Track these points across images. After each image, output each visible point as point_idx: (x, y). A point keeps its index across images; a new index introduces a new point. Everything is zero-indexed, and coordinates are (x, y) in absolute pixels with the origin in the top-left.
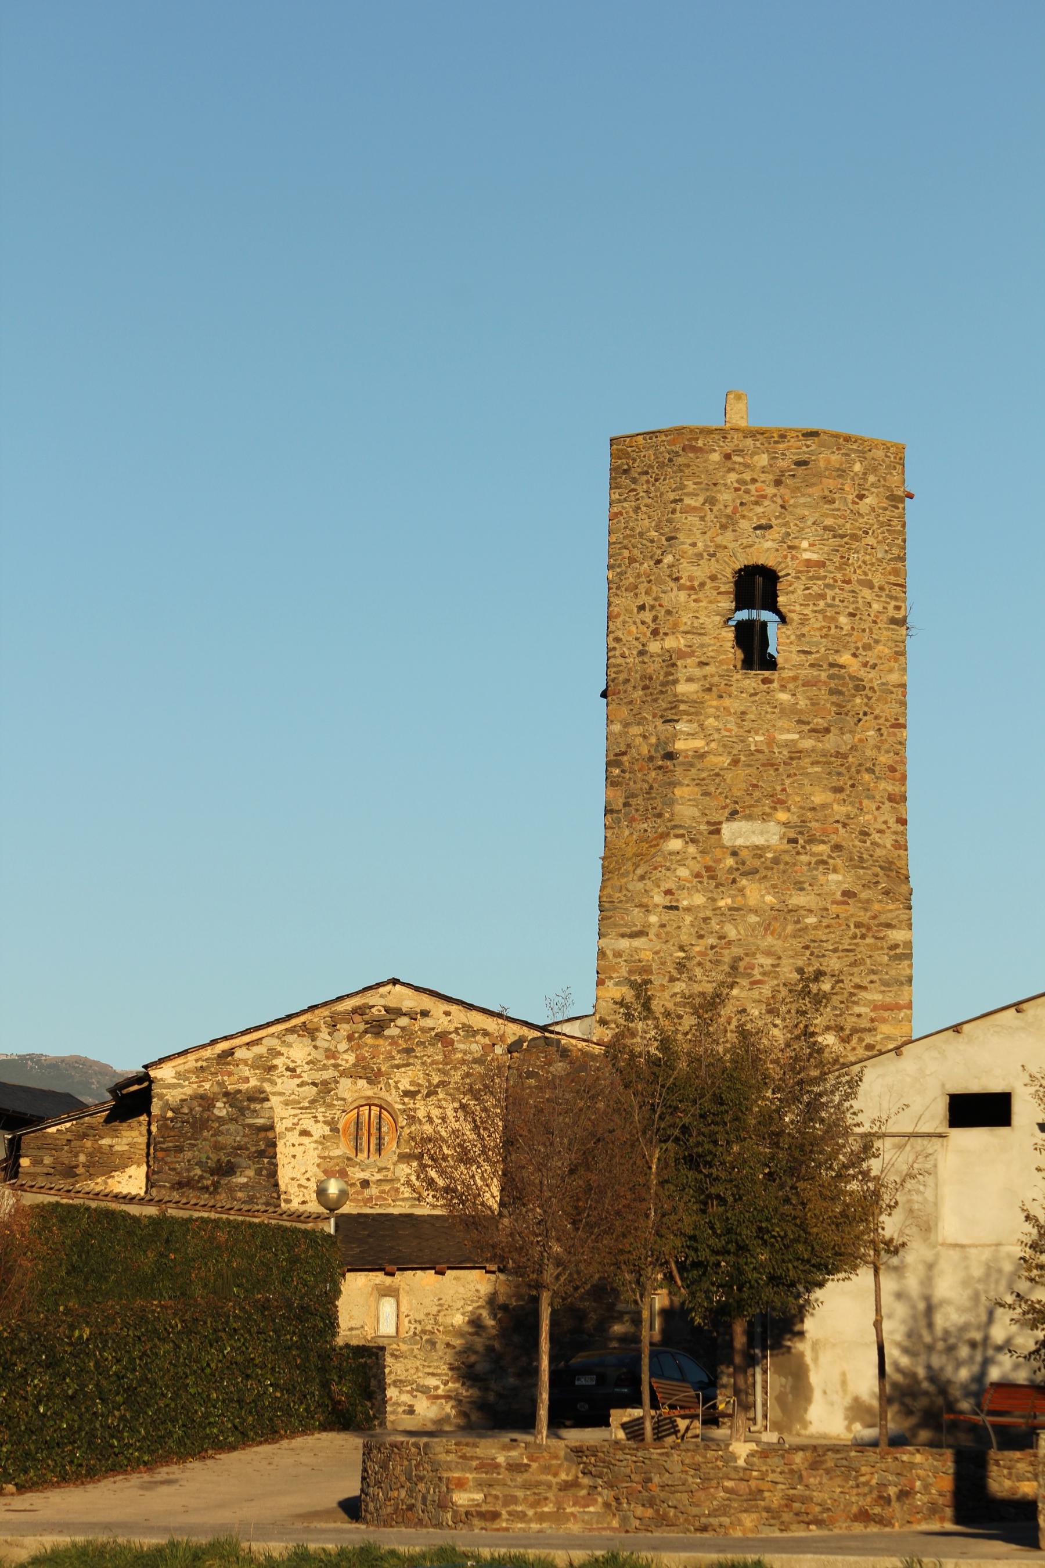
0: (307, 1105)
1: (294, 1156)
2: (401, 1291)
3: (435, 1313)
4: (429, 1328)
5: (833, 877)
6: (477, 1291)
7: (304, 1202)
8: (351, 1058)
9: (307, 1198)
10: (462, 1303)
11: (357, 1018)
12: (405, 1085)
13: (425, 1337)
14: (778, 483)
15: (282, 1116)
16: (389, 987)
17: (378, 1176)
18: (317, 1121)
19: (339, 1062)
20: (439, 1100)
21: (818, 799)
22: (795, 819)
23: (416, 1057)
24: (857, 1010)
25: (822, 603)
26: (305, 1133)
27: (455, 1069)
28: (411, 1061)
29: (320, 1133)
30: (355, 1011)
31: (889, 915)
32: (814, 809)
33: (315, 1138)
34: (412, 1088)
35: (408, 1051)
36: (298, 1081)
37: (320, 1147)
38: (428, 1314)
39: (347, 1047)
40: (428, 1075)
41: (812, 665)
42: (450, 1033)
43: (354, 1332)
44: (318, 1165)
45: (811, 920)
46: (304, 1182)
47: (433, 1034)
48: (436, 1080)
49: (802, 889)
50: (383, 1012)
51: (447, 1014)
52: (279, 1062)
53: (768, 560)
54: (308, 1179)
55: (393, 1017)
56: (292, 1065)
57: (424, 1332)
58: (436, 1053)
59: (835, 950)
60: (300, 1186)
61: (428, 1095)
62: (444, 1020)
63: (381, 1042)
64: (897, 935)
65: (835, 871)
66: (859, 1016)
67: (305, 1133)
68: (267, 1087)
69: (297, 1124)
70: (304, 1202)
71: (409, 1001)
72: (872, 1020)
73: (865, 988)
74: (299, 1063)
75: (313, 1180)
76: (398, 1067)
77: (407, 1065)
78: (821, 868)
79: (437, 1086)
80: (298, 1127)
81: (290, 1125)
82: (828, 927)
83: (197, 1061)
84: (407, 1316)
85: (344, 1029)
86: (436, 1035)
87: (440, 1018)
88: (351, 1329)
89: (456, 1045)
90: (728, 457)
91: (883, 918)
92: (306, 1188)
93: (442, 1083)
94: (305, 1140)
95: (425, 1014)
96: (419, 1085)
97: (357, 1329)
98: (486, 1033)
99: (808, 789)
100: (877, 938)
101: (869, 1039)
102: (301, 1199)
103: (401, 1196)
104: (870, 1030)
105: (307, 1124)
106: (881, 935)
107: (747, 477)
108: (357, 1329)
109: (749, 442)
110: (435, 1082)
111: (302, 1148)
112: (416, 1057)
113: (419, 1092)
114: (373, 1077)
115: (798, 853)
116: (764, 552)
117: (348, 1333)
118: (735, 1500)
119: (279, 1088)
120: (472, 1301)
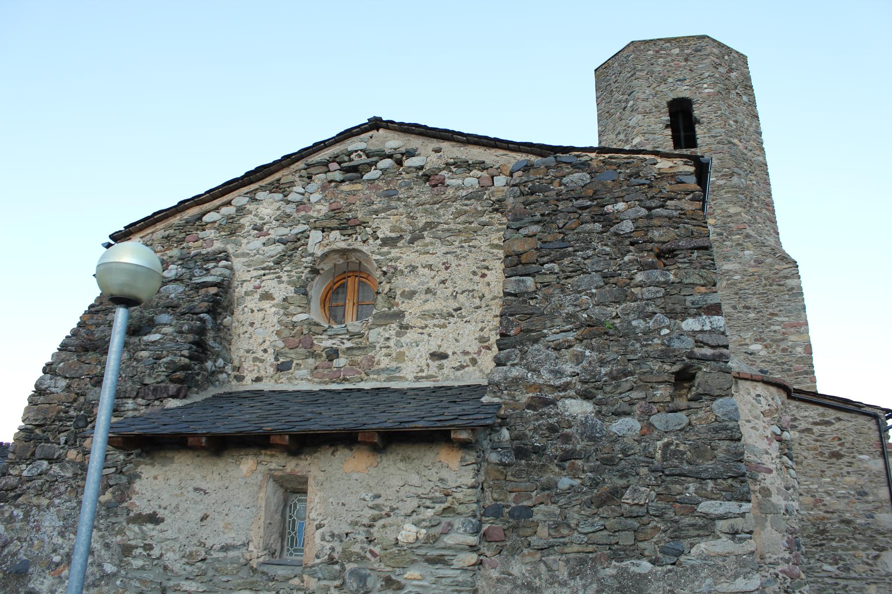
0: (272, 264)
1: (252, 324)
2: (311, 482)
3: (366, 521)
4: (356, 548)
5: (746, 252)
6: (441, 480)
7: (258, 379)
8: (324, 209)
9: (263, 373)
10: (415, 503)
11: (334, 166)
12: (385, 231)
13: (349, 566)
14: (686, 60)
15: (245, 278)
16: (373, 133)
17: (349, 344)
18: (281, 282)
19: (311, 213)
20: (426, 245)
21: (732, 210)
22: (719, 222)
23: (399, 199)
24: (773, 328)
25: (719, 112)
26: (267, 296)
27: (445, 206)
28: (393, 204)
29: (283, 294)
30: (334, 159)
31: (785, 271)
32: (730, 216)
33: (275, 302)
34: (393, 235)
35: (389, 195)
36: (263, 239)
37: (282, 311)
38: (355, 524)
39: (320, 196)
40: (412, 218)
41: (718, 143)
42: (440, 170)
43: (231, 554)
44: (278, 333)
45: (737, 277)
46: (260, 354)
47: (421, 173)
48: (422, 221)
49: (729, 261)
50: (364, 157)
51: (437, 151)
52: (246, 221)
53: (686, 94)
54: (265, 351)
55: (374, 159)
56: (259, 222)
57: (348, 556)
58: (424, 192)
59: (754, 294)
60: (255, 359)
61: (411, 242)
62: (434, 157)
63: (358, 187)
64: (791, 282)
65: (748, 249)
66: (775, 331)
67: (267, 296)
68: (230, 248)
69: (259, 288)
70: (258, 379)
71: (393, 142)
72: (784, 334)
73: (776, 315)
74: (267, 218)
75: (271, 351)
76: (376, 212)
77: (389, 208)
78: (739, 248)
79: (424, 229)
80: (259, 291)
81: (251, 288)
82: (748, 280)
83: (165, 229)
84: (319, 526)
85: (320, 178)
86: (424, 175)
87: (427, 155)
88: (225, 548)
89: (448, 182)
90: (657, 52)
91: (781, 274)
92: (262, 361)
93: (429, 225)
94: (266, 304)
95: (410, 154)
96: (402, 230)
97: (234, 547)
98: (482, 166)
99: (725, 206)
100: (780, 285)
101: (783, 345)
102: (255, 375)
103: (376, 367)
104: (783, 340)
105: (269, 284)
106: (782, 283)
107: (669, 59)
108: (234, 547)
109: (668, 44)
110: (421, 225)
111: (261, 314)
112: (399, 199)
113: (401, 237)
114: (347, 226)
115: (724, 241)
116: (683, 91)
117: (221, 555)
118: (268, 274)
119: (244, 248)
120: (435, 500)
